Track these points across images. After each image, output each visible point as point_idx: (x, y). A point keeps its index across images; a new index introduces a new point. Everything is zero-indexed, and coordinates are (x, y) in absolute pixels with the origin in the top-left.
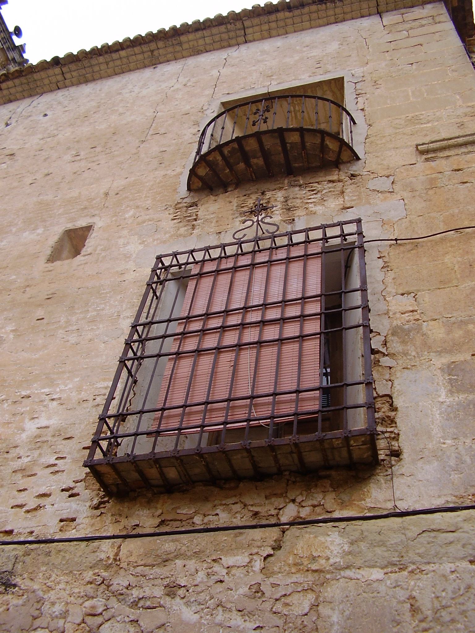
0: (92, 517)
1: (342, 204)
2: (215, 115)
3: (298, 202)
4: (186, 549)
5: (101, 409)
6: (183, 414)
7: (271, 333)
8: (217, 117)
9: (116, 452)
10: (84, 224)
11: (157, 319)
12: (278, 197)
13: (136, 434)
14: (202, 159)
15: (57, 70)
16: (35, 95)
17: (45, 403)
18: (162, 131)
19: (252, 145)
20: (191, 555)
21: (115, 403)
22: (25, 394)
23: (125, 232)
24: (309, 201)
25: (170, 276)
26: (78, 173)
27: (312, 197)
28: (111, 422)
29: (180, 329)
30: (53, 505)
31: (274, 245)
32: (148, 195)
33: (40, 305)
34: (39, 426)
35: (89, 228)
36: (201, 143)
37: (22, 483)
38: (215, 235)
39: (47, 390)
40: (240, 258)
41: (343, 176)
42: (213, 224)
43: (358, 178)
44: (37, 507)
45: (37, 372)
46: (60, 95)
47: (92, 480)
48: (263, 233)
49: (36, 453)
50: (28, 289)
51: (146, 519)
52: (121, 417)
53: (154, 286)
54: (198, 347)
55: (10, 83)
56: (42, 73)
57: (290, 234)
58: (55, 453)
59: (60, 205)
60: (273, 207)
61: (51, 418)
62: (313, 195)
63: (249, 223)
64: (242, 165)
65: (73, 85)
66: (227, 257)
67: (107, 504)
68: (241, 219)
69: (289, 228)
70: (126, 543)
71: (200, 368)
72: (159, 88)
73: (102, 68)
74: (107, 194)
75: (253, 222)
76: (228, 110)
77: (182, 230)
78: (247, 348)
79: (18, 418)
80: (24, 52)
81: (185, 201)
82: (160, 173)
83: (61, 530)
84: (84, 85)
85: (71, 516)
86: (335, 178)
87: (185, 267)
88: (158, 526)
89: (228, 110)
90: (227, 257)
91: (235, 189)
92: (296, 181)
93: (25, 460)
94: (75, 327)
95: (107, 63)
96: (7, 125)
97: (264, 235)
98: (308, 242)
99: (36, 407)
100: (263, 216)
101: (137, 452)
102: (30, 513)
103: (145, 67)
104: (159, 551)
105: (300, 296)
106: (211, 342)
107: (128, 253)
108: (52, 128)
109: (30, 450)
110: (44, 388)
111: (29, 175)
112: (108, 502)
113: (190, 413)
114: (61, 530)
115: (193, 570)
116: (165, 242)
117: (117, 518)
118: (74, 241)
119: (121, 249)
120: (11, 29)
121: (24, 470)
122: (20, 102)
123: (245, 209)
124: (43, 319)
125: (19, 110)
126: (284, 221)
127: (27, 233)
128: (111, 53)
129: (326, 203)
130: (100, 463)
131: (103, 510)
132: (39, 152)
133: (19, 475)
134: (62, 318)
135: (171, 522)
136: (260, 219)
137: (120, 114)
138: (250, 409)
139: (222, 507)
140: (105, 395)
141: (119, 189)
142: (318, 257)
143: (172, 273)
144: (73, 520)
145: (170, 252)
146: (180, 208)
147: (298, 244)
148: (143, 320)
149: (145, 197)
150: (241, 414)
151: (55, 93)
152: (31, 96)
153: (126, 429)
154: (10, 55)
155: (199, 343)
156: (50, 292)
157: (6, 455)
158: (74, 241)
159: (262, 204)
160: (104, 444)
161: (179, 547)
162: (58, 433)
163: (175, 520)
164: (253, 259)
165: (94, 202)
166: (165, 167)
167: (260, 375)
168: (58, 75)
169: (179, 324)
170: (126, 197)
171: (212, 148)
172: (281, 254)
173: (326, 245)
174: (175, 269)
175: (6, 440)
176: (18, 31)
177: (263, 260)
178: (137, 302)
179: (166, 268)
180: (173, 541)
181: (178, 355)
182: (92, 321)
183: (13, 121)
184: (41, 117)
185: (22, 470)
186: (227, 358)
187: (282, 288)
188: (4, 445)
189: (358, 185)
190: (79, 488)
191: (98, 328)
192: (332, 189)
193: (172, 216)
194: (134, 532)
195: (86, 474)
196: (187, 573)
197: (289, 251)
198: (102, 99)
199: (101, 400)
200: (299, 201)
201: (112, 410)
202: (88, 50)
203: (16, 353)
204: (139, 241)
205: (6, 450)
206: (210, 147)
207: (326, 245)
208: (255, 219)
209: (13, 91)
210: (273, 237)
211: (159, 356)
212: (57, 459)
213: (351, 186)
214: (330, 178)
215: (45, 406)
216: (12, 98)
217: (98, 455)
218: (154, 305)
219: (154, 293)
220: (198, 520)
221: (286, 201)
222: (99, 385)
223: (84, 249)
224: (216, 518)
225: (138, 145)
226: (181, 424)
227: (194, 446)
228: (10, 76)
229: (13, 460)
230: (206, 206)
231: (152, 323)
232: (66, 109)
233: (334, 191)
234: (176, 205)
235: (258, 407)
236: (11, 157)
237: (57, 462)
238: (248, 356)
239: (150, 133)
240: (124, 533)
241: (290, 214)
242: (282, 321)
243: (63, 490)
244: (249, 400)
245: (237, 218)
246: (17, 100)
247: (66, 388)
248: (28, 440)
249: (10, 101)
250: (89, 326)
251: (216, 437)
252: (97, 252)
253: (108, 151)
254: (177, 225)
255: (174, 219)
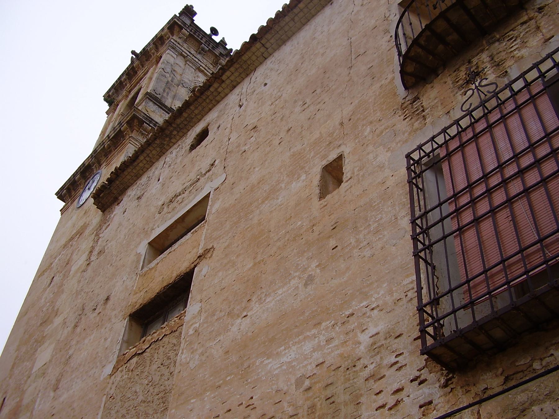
0: (445, 395)
1: (542, 38)
2: (398, 17)
3: (503, 55)
4: (537, 395)
5: (415, 301)
6: (487, 279)
7: (532, 178)
8: (401, 17)
9: (443, 333)
10: (335, 156)
11: (429, 208)
12: (484, 59)
13: (454, 312)
14: (406, 59)
15: (258, 45)
16: (250, 73)
17: (368, 314)
18: (362, 51)
19: (442, 25)
20: (544, 398)
21: (424, 291)
22: (349, 313)
23: (371, 148)
24: (512, 49)
25: (424, 168)
26: (312, 117)
27: (513, 45)
28: (428, 309)
29: (452, 208)
30: (409, 396)
31: (500, 102)
32: (375, 109)
33: (329, 237)
34: (370, 335)
35: (340, 158)
36: (398, 46)
37: (376, 387)
38: (445, 116)
39: (365, 303)
40: (476, 125)
41: (532, 14)
42: (440, 108)
43: (546, 8)
44: (397, 402)
45: (351, 292)
46: (269, 64)
47: (432, 364)
48: (486, 95)
49: (378, 358)
50: (314, 228)
51: (492, 381)
52: (435, 302)
53: (414, 181)
54: (474, 216)
55: (228, 73)
56: (248, 53)
57: (509, 86)
58: (393, 352)
59: (310, 150)
60: (484, 70)
61: (378, 325)
62: (513, 42)
63: (470, 92)
64: (441, 47)
65: (275, 50)
66: (464, 130)
67: (454, 380)
68: (460, 92)
69: (506, 81)
70: (483, 407)
71: (483, 234)
72: (343, 18)
73: (291, 25)
74: (342, 124)
75: (473, 90)
76: (408, 7)
77: (416, 125)
78: (517, 200)
79: (351, 335)
80: (226, 44)
81: (407, 99)
82: (377, 86)
83: (423, 415)
84: (283, 46)
85: (427, 401)
86: (525, 18)
87: (433, 154)
88: (504, 383)
89: (408, 7)
90: (464, 130)
91: (444, 69)
92: (493, 38)
93: (372, 367)
94: (365, 243)
95: (293, 19)
96: (240, 106)
97: (487, 97)
98: (528, 85)
99: (362, 320)
100: (479, 81)
101: (461, 326)
102: (393, 410)
103: (323, 7)
104: (514, 404)
105: (543, 135)
106: (483, 207)
107: (381, 165)
108: (275, 92)
109: (371, 357)
110: (361, 302)
111: (275, 137)
112: (453, 377)
113: (493, 276)
114: (423, 415)
115: (551, 411)
116: (406, 141)
117: (466, 387)
118: (333, 173)
119: (374, 163)
120: (208, 32)
121: (373, 375)
122: (242, 84)
123: (461, 82)
124: (337, 246)
125: (244, 90)
126: (499, 77)
127: (294, 183)
128: (292, 10)
129: (528, 44)
130: (433, 347)
131: (452, 386)
132: (275, 116)
133: (372, 381)
134: (351, 240)
135: (515, 376)
136: (477, 85)
137: (323, 55)
138: (544, 252)
139: (554, 347)
140: (413, 288)
141: (349, 115)
142: (543, 94)
143: (424, 164)
144: (430, 403)
145: (415, 147)
146: (406, 107)
147: (520, 91)
148: (418, 214)
149: (374, 111)
150: (537, 259)
151: (265, 63)
152: (247, 75)
153: (443, 310)
154: (217, 52)
155: (474, 213)
156: (333, 223)
157: (354, 369)
158: (333, 173)
159: (473, 71)
160: (430, 330)
161: (530, 395)
162: (388, 335)
163: (517, 373)
164: (487, 121)
165: (335, 134)
166: (378, 79)
167: (539, 219)
168: (260, 48)
169: (449, 203)
170: (358, 119)
171: (409, 45)
172: (510, 106)
173: (546, 80)
174: (425, 160)
175: (349, 356)
176: (214, 31)
177: (496, 119)
178: (406, 200)
179: (418, 162)
180: (523, 391)
181: (461, 230)
182: (377, 231)
183: (244, 101)
184: (263, 88)
185: (372, 376)
186: (503, 216)
187: (524, 135)
188: (350, 361)
189: (549, 14)
190: (425, 374)
191: (384, 236)
192: (528, 30)
193: (402, 117)
194: (486, 396)
195: (425, 360)
196: (546, 415)
197: (515, 101)
198: (302, 50)
199: (412, 294)
200: (503, 54)
201: (425, 300)
202: (248, 40)
203: (328, 283)
204: (386, 150)
205: (353, 365)
206: (407, 45)
207: (546, 80)
208: (473, 87)
209: (232, 78)
210: (496, 95)
211: (444, 237)
212: (396, 357)
213: (543, 19)
214: (521, 21)
215: (369, 317)
216: (235, 83)
217: (430, 341)
218: (421, 197)
219: (417, 187)
220: (537, 365)
221: (493, 59)
222: (405, 282)
223: (344, 176)
224: (552, 358)
225: (348, 73)
226: (489, 288)
227: (507, 302)
228: (225, 67)
229: (361, 370)
230: (427, 95)
231: (426, 213)
232: (279, 72)
233: (530, 31)
234: (402, 106)
235: (550, 247)
236: (255, 130)
237: (397, 359)
238: (521, 207)
239: (353, 58)
240: (478, 399)
241: (501, 68)
242: (520, 173)
243: (412, 381)
244: (539, 244)
245: (457, 93)
246: (239, 83)
247: (380, 295)
248: (367, 350)
249: (234, 87)
250: (376, 237)
251: (522, 288)
252: (356, 174)
253: (327, 89)
254: (410, 122)
255: (406, 118)
